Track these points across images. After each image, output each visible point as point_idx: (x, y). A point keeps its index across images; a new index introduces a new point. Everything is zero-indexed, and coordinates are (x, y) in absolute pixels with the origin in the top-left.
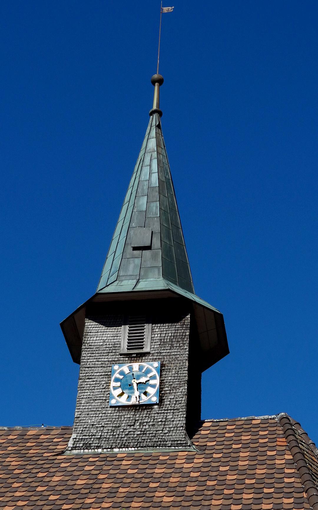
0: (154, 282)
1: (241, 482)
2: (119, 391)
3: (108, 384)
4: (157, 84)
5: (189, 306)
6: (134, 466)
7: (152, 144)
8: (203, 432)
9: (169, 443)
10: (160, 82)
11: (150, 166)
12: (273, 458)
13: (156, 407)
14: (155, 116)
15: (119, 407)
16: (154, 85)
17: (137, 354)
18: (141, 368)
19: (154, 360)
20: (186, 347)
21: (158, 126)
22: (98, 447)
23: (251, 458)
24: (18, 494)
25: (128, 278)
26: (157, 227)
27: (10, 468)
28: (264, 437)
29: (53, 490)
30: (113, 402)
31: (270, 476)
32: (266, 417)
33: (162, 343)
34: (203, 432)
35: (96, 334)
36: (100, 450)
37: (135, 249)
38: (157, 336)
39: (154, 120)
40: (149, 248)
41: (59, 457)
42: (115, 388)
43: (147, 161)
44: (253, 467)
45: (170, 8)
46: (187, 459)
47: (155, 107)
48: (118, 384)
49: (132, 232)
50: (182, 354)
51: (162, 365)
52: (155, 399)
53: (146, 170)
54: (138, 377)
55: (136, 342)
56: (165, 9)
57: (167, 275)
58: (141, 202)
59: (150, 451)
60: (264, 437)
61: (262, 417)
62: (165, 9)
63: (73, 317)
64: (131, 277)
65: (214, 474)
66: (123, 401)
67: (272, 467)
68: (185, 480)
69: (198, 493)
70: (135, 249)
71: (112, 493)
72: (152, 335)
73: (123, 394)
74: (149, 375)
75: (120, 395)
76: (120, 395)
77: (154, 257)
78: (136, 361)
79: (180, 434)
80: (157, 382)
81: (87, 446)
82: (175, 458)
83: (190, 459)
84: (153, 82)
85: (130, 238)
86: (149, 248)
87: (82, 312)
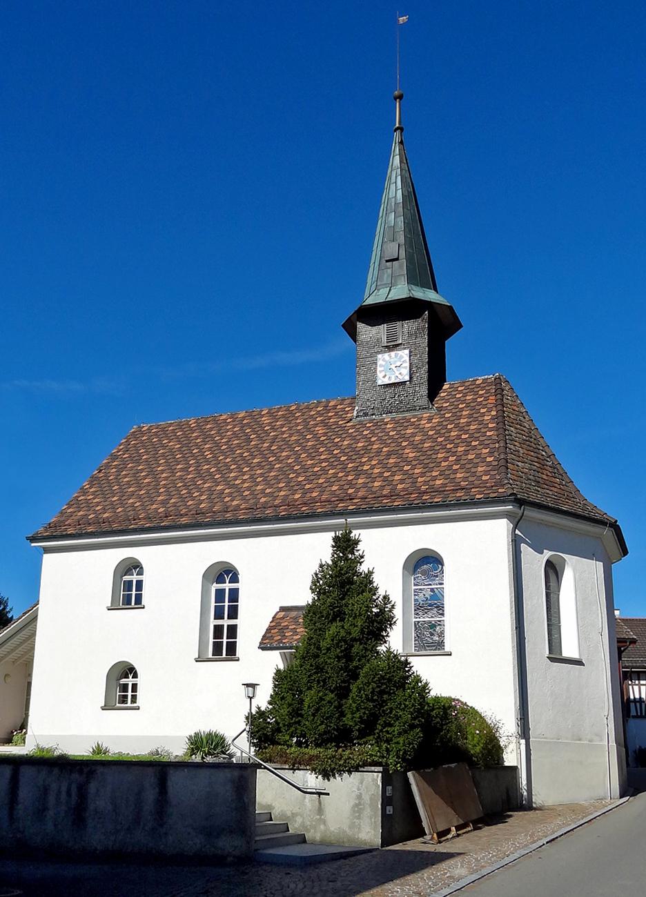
0: (401, 291)
1: (459, 437)
2: (383, 374)
3: (375, 369)
4: (398, 100)
5: (429, 305)
6: (394, 429)
7: (397, 161)
8: (442, 395)
9: (418, 408)
10: (400, 97)
11: (396, 183)
12: (483, 415)
13: (408, 383)
14: (398, 132)
15: (384, 385)
16: (396, 100)
17: (393, 345)
18: (396, 356)
19: (405, 349)
20: (426, 337)
21: (401, 143)
22: (372, 415)
23: (470, 416)
24: (322, 457)
25: (383, 286)
26: (401, 239)
27: (329, 424)
28: (481, 396)
29: (343, 452)
30: (380, 382)
31: (478, 431)
32: (486, 377)
33: (410, 335)
34: (442, 395)
35: (366, 332)
36: (374, 417)
37: (387, 261)
38: (405, 330)
39: (397, 136)
40: (397, 259)
41: (348, 424)
42: (380, 372)
43: (393, 179)
44: (469, 424)
45: (405, 18)
46: (428, 419)
47: (397, 125)
48: (382, 369)
49: (384, 247)
50: (424, 341)
51: (410, 352)
52: (407, 378)
53: (393, 186)
54: (395, 362)
55: (392, 337)
56: (403, 19)
57: (412, 280)
58: (390, 218)
59: (406, 415)
60: (481, 396)
61: (483, 377)
62: (403, 19)
63: (91, 773)
64: (385, 285)
65: (444, 431)
66: (386, 381)
67: (481, 423)
68: (425, 437)
69: (431, 448)
70: (387, 261)
71: (379, 451)
72: (405, 328)
73: (385, 376)
74: (402, 360)
75: (384, 377)
76: (384, 377)
77: (401, 267)
78: (393, 351)
79: (424, 401)
80: (407, 365)
81: (366, 415)
82: (420, 419)
83: (430, 419)
84: (395, 99)
85: (384, 252)
86: (397, 259)
87: (355, 315)
